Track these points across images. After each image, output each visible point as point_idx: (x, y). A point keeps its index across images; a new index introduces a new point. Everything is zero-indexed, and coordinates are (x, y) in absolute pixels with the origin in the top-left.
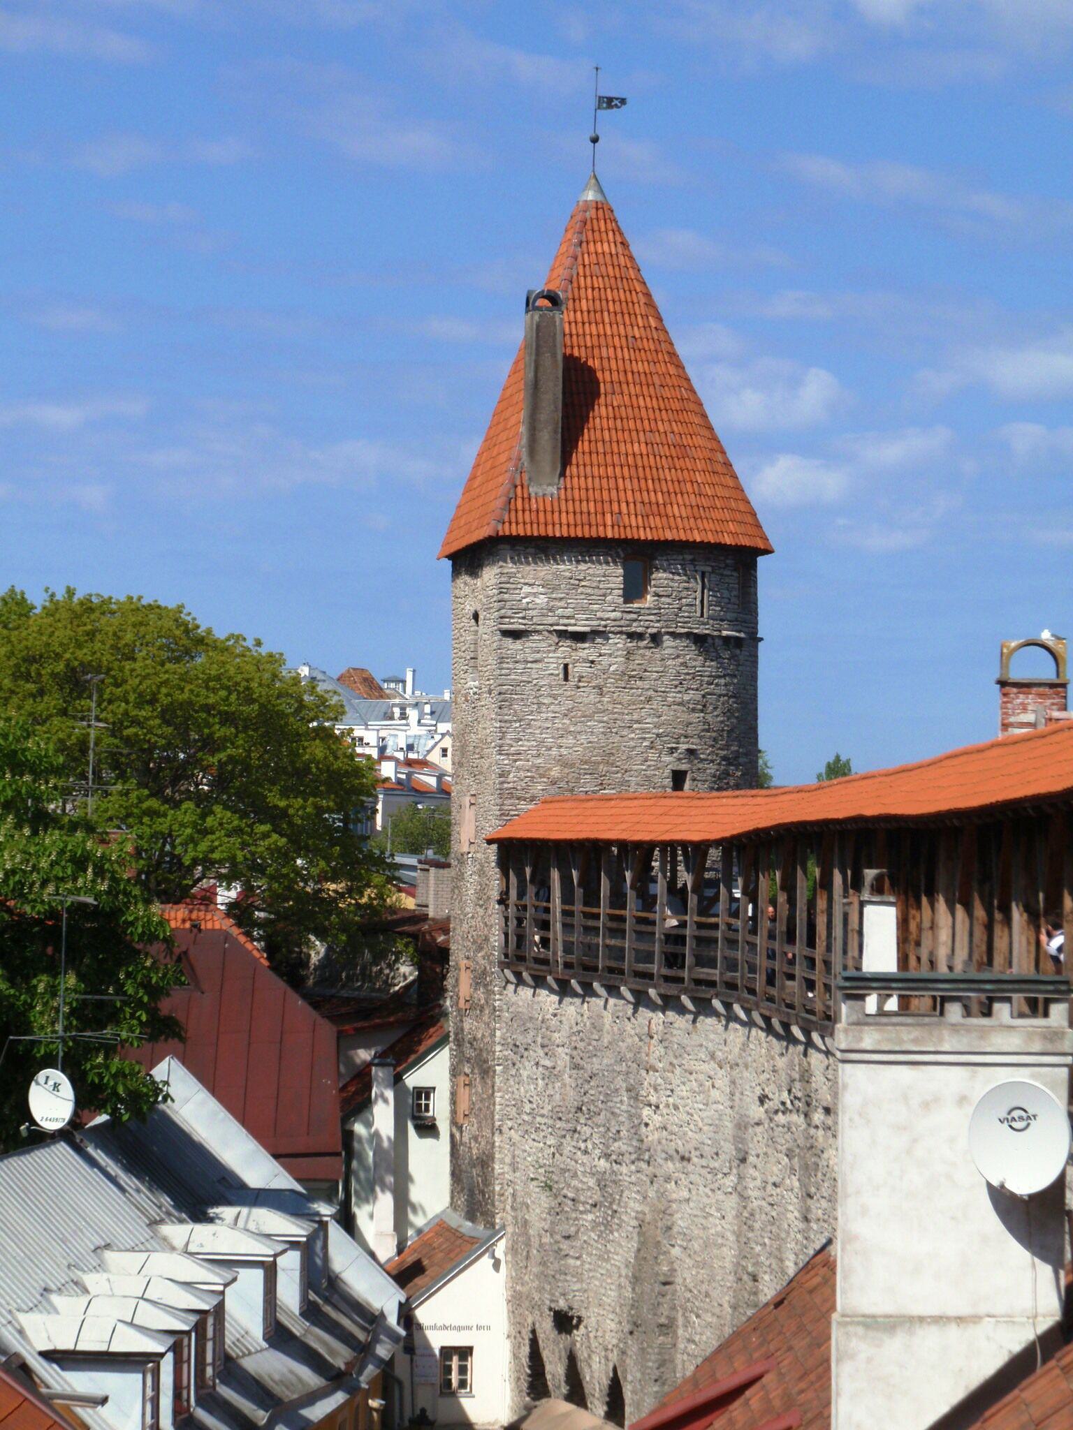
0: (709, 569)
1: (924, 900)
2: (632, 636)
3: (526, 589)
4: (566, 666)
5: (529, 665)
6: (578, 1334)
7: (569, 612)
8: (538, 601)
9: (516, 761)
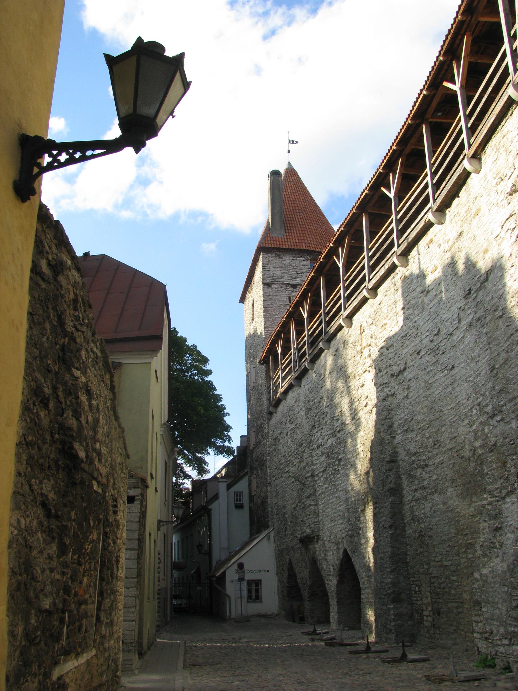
1: (461, 266)
4: (289, 298)
6: (317, 547)
7: (289, 278)
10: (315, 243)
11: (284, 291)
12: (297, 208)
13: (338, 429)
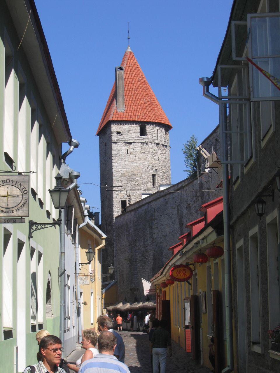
0: (159, 129)
2: (142, 143)
4: (127, 150)
5: (119, 150)
7: (128, 138)
9: (116, 172)
13: (146, 246)
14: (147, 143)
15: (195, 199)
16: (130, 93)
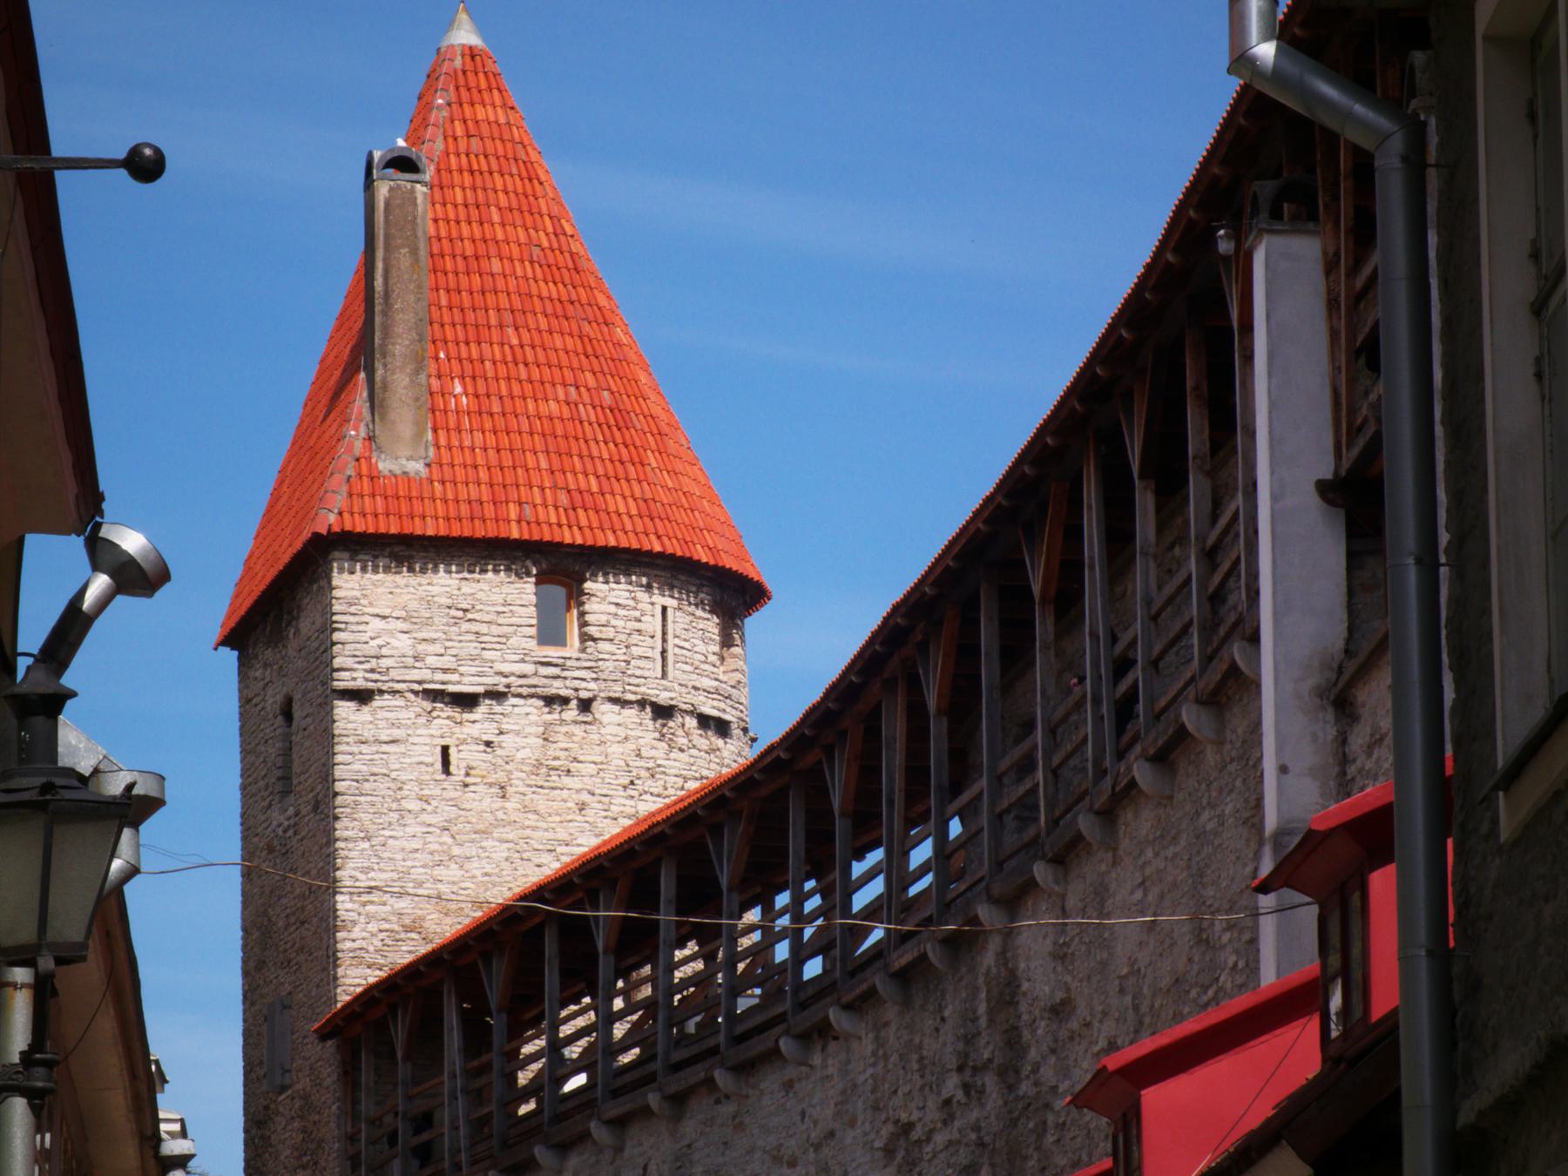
2: (550, 700)
3: (377, 624)
4: (445, 750)
5: (385, 748)
8: (394, 642)
9: (364, 904)
10: (563, 499)
11: (422, 720)
12: (490, 298)
14: (585, 705)
15: (952, 1086)
16: (467, 343)
